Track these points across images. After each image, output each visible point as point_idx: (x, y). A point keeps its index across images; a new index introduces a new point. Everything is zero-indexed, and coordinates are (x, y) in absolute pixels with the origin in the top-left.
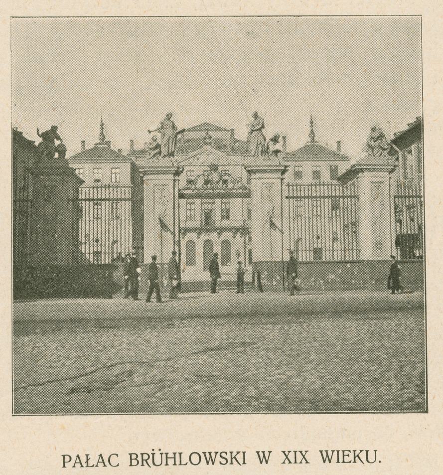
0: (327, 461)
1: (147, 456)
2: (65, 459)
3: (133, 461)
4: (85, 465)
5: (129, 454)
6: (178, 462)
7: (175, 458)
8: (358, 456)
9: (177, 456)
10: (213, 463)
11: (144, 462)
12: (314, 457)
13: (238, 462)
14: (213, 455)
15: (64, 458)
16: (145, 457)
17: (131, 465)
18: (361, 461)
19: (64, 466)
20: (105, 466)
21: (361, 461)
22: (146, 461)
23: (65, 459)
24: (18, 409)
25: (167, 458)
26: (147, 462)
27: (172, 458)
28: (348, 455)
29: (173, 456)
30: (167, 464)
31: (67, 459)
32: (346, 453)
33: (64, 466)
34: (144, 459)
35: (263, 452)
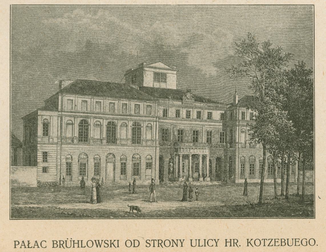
0: (99, 246)
1: (284, 240)
2: (16, 243)
3: (54, 244)
4: (27, 247)
5: (191, 240)
6: (80, 246)
7: (79, 244)
8: (250, 242)
9: (80, 242)
10: (100, 247)
11: (61, 245)
12: (243, 242)
13: (114, 246)
14: (100, 242)
15: (15, 242)
16: (62, 243)
17: (53, 247)
18: (252, 245)
19: (15, 247)
20: (38, 247)
21: (252, 245)
22: (62, 245)
23: (16, 243)
24: (14, 9)
25: (74, 243)
26: (236, 244)
27: (75, 243)
28: (278, 242)
29: (78, 242)
30: (74, 247)
31: (17, 243)
32: (297, 240)
33: (15, 247)
34: (159, 243)
35: (98, 241)
